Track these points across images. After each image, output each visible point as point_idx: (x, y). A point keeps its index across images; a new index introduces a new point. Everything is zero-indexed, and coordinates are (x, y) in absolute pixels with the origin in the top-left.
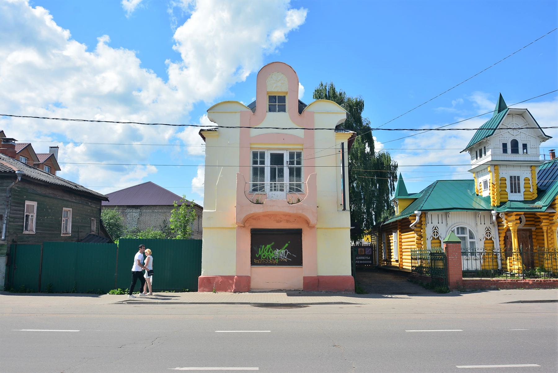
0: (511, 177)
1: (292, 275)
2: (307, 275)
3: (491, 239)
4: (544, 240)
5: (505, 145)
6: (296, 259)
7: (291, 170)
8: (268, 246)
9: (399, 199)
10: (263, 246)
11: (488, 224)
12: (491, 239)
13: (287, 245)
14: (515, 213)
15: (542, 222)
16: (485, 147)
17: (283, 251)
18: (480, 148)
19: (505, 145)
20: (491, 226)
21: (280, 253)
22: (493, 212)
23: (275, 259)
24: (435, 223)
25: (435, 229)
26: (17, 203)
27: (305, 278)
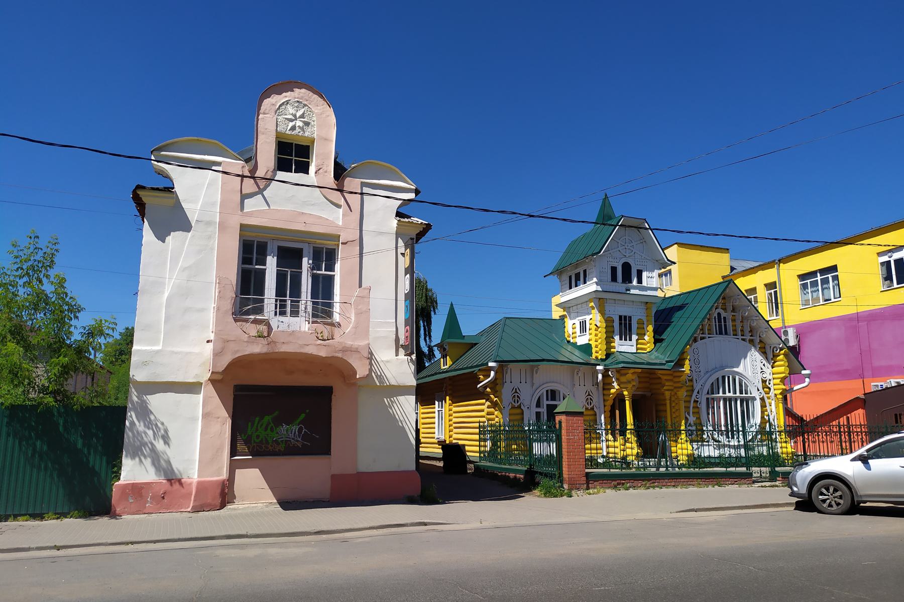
0: (620, 317)
1: (311, 471)
2: (336, 470)
3: (592, 409)
4: (666, 411)
5: (614, 270)
6: (318, 442)
7: (315, 278)
8: (267, 418)
9: (449, 343)
10: (257, 419)
11: (589, 387)
12: (592, 409)
13: (303, 416)
14: (632, 371)
15: (664, 385)
16: (585, 271)
17: (295, 428)
18: (577, 271)
19: (614, 270)
20: (594, 389)
21: (290, 431)
22: (598, 368)
23: (278, 444)
24: (516, 384)
25: (516, 392)
26: (777, 308)
27: (333, 476)
